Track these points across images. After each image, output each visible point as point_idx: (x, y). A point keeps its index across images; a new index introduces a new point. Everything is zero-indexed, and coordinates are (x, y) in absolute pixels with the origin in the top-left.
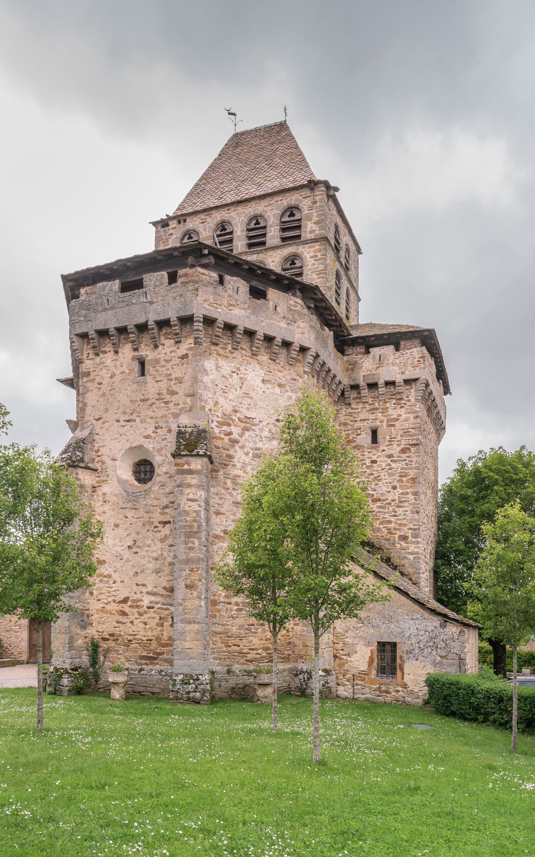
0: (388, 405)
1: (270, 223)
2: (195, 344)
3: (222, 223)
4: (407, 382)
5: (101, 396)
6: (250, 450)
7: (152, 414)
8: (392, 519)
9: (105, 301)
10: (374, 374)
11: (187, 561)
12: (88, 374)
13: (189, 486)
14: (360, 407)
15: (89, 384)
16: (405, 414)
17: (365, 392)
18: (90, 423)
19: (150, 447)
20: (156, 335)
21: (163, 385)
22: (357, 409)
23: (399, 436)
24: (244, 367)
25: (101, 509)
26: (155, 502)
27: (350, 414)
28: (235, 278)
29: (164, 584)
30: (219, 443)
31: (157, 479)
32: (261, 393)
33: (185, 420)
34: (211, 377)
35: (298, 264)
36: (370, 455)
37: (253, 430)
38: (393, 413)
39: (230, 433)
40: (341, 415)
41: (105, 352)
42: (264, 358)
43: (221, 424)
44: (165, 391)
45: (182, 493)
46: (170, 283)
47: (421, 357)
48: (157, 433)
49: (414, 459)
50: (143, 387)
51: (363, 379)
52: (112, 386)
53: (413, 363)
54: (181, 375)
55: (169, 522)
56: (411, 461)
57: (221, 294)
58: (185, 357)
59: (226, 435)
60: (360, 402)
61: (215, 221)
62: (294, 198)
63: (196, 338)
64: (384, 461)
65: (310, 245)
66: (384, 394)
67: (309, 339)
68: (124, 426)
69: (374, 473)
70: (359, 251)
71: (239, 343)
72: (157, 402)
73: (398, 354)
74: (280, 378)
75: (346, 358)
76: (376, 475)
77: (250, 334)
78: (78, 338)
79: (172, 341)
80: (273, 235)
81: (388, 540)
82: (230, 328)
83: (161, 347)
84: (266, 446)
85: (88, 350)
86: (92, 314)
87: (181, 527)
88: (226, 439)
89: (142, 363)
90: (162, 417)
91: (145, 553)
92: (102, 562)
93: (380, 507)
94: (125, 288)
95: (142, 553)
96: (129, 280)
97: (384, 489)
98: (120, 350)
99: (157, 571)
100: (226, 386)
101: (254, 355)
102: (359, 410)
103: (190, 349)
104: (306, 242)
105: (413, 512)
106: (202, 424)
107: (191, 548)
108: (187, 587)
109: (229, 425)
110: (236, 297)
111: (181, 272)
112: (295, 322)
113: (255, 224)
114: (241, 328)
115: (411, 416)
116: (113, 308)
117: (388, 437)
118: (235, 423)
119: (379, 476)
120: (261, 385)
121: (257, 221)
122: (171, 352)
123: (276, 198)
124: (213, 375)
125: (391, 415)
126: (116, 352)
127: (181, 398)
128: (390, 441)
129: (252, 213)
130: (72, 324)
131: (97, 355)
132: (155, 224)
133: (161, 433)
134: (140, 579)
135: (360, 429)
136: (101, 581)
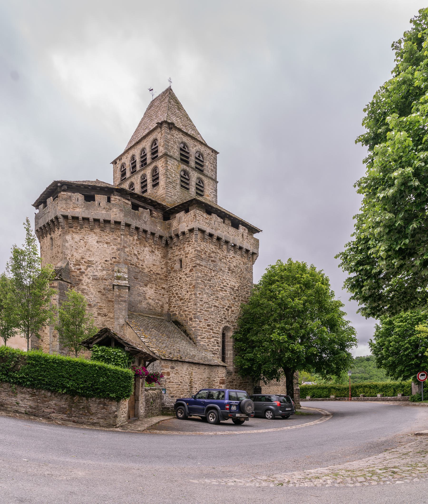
0: (185, 245)
4: (191, 231)
8: (187, 309)
30: (74, 274)
32: (96, 248)
37: (92, 267)
39: (80, 269)
42: (98, 230)
57: (69, 203)
59: (78, 270)
67: (120, 217)
70: (216, 153)
81: (185, 321)
82: (75, 218)
84: (100, 274)
88: (78, 272)
93: (182, 303)
101: (92, 230)
109: (80, 265)
110: (77, 203)
112: (111, 209)
114: (80, 218)
115: (193, 250)
120: (96, 244)
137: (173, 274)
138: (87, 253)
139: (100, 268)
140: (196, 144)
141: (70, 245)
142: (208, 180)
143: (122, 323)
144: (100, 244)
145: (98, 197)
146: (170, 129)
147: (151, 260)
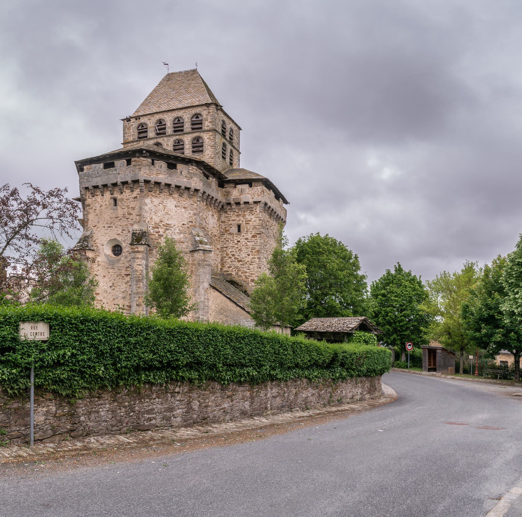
0: (246, 213)
4: (255, 203)
7: (121, 224)
8: (247, 271)
11: (137, 293)
12: (89, 205)
13: (138, 258)
15: (89, 210)
16: (254, 218)
17: (234, 206)
19: (120, 239)
21: (126, 210)
25: (97, 269)
26: (123, 265)
27: (227, 217)
29: (127, 304)
30: (153, 237)
31: (123, 254)
33: (136, 227)
34: (149, 206)
35: (201, 141)
36: (237, 238)
38: (248, 217)
39: (159, 232)
41: (97, 195)
42: (176, 195)
43: (154, 228)
44: (126, 213)
45: (134, 262)
46: (127, 165)
49: (259, 241)
53: (258, 193)
55: (129, 275)
58: (136, 197)
61: (156, 119)
67: (199, 186)
70: (240, 129)
73: (250, 189)
75: (224, 190)
77: (168, 185)
79: (130, 190)
80: (187, 127)
82: (157, 184)
83: (124, 193)
85: (88, 194)
87: (134, 277)
88: (157, 235)
89: (115, 200)
91: (118, 289)
92: (97, 294)
95: (117, 289)
96: (108, 162)
97: (244, 255)
99: (124, 298)
101: (171, 195)
103: (138, 194)
104: (205, 131)
105: (258, 268)
106: (144, 229)
107: (139, 287)
108: (137, 305)
109: (158, 228)
110: (160, 170)
111: (133, 159)
115: (257, 219)
116: (100, 176)
120: (175, 208)
123: (188, 110)
124: (150, 206)
126: (103, 195)
127: (134, 217)
130: (81, 183)
131: (93, 196)
132: (122, 120)
134: (116, 302)
136: (97, 303)
139: (178, 231)
143: (207, 287)
144: (178, 208)
145: (180, 166)
146: (217, 110)
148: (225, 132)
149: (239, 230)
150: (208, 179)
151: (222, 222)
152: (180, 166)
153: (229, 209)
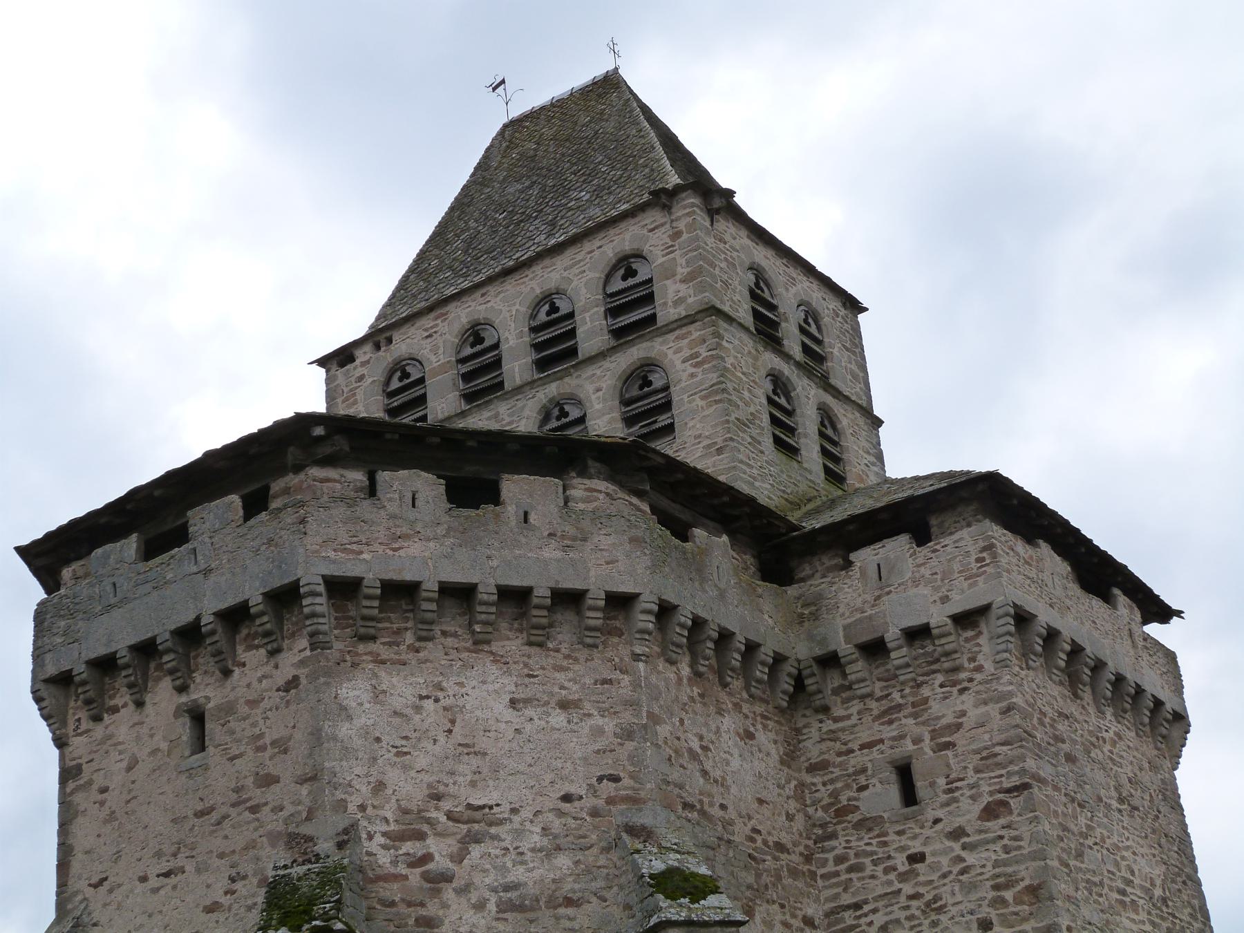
0: (925, 691)
1: (579, 306)
2: (312, 650)
3: (472, 327)
4: (967, 619)
5: (106, 822)
6: (487, 894)
9: (109, 588)
10: (870, 617)
14: (854, 710)
17: (858, 668)
18: (80, 897)
20: (223, 645)
21: (245, 765)
22: (849, 717)
23: (970, 772)
24: (454, 679)
27: (832, 736)
28: (403, 473)
30: (392, 891)
32: (510, 734)
34: (361, 721)
36: (904, 840)
39: (427, 858)
40: (808, 744)
41: (115, 710)
42: (511, 644)
43: (396, 838)
47: (984, 549)
48: (233, 892)
49: (1024, 830)
50: (200, 779)
51: (846, 637)
52: (130, 791)
54: (284, 733)
56: (1016, 839)
57: (367, 516)
58: (293, 683)
59: (411, 865)
60: (853, 698)
62: (628, 236)
63: (312, 635)
64: (945, 852)
65: (677, 332)
66: (908, 665)
68: (158, 889)
69: (922, 890)
70: (854, 306)
71: (432, 623)
72: (233, 812)
73: (924, 551)
74: (562, 687)
75: (792, 591)
76: (929, 897)
77: (460, 595)
78: (52, 689)
79: (263, 651)
80: (592, 330)
82: (400, 593)
83: (237, 671)
84: (537, 874)
86: (80, 623)
88: (415, 876)
89: (198, 717)
90: (246, 848)
94: (150, 551)
98: (148, 698)
100: (406, 738)
101: (479, 643)
102: (854, 720)
103: (302, 663)
104: (670, 328)
109: (421, 836)
110: (411, 514)
112: (585, 540)
113: (548, 314)
115: (993, 710)
117: (942, 781)
118: (439, 828)
119: (936, 898)
120: (509, 714)
121: (553, 305)
122: (260, 681)
125: (938, 718)
126: (140, 704)
128: (950, 791)
129: (538, 291)
130: (38, 655)
131: (97, 719)
132: (322, 362)
133: (244, 892)
135: (864, 770)
137: (847, 840)
138: (461, 768)
139: (536, 839)
140: (795, 276)
141: (365, 732)
142: (849, 415)
144: (529, 712)
145: (514, 487)
146: (712, 213)
147: (749, 778)
148: (775, 325)
149: (909, 796)
150: (684, 538)
151: (812, 769)
152: (514, 487)
153: (836, 692)
